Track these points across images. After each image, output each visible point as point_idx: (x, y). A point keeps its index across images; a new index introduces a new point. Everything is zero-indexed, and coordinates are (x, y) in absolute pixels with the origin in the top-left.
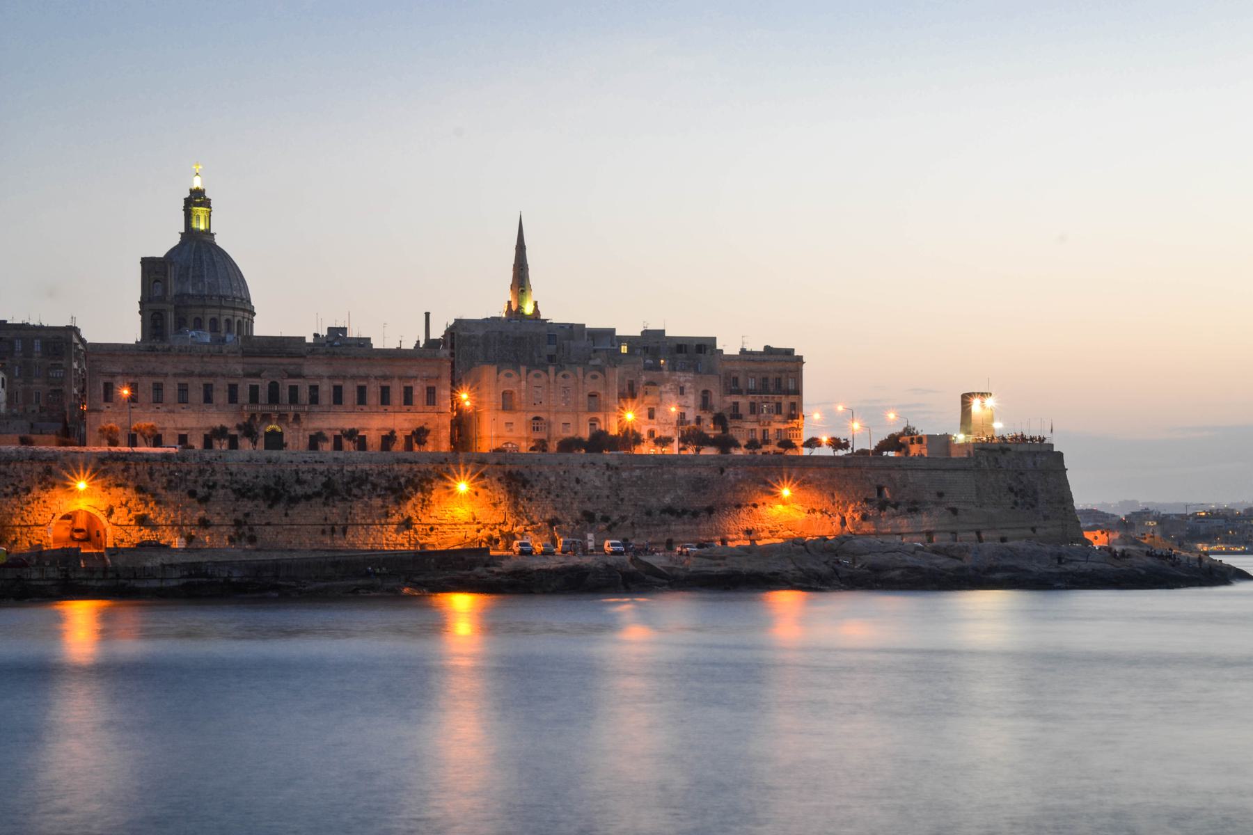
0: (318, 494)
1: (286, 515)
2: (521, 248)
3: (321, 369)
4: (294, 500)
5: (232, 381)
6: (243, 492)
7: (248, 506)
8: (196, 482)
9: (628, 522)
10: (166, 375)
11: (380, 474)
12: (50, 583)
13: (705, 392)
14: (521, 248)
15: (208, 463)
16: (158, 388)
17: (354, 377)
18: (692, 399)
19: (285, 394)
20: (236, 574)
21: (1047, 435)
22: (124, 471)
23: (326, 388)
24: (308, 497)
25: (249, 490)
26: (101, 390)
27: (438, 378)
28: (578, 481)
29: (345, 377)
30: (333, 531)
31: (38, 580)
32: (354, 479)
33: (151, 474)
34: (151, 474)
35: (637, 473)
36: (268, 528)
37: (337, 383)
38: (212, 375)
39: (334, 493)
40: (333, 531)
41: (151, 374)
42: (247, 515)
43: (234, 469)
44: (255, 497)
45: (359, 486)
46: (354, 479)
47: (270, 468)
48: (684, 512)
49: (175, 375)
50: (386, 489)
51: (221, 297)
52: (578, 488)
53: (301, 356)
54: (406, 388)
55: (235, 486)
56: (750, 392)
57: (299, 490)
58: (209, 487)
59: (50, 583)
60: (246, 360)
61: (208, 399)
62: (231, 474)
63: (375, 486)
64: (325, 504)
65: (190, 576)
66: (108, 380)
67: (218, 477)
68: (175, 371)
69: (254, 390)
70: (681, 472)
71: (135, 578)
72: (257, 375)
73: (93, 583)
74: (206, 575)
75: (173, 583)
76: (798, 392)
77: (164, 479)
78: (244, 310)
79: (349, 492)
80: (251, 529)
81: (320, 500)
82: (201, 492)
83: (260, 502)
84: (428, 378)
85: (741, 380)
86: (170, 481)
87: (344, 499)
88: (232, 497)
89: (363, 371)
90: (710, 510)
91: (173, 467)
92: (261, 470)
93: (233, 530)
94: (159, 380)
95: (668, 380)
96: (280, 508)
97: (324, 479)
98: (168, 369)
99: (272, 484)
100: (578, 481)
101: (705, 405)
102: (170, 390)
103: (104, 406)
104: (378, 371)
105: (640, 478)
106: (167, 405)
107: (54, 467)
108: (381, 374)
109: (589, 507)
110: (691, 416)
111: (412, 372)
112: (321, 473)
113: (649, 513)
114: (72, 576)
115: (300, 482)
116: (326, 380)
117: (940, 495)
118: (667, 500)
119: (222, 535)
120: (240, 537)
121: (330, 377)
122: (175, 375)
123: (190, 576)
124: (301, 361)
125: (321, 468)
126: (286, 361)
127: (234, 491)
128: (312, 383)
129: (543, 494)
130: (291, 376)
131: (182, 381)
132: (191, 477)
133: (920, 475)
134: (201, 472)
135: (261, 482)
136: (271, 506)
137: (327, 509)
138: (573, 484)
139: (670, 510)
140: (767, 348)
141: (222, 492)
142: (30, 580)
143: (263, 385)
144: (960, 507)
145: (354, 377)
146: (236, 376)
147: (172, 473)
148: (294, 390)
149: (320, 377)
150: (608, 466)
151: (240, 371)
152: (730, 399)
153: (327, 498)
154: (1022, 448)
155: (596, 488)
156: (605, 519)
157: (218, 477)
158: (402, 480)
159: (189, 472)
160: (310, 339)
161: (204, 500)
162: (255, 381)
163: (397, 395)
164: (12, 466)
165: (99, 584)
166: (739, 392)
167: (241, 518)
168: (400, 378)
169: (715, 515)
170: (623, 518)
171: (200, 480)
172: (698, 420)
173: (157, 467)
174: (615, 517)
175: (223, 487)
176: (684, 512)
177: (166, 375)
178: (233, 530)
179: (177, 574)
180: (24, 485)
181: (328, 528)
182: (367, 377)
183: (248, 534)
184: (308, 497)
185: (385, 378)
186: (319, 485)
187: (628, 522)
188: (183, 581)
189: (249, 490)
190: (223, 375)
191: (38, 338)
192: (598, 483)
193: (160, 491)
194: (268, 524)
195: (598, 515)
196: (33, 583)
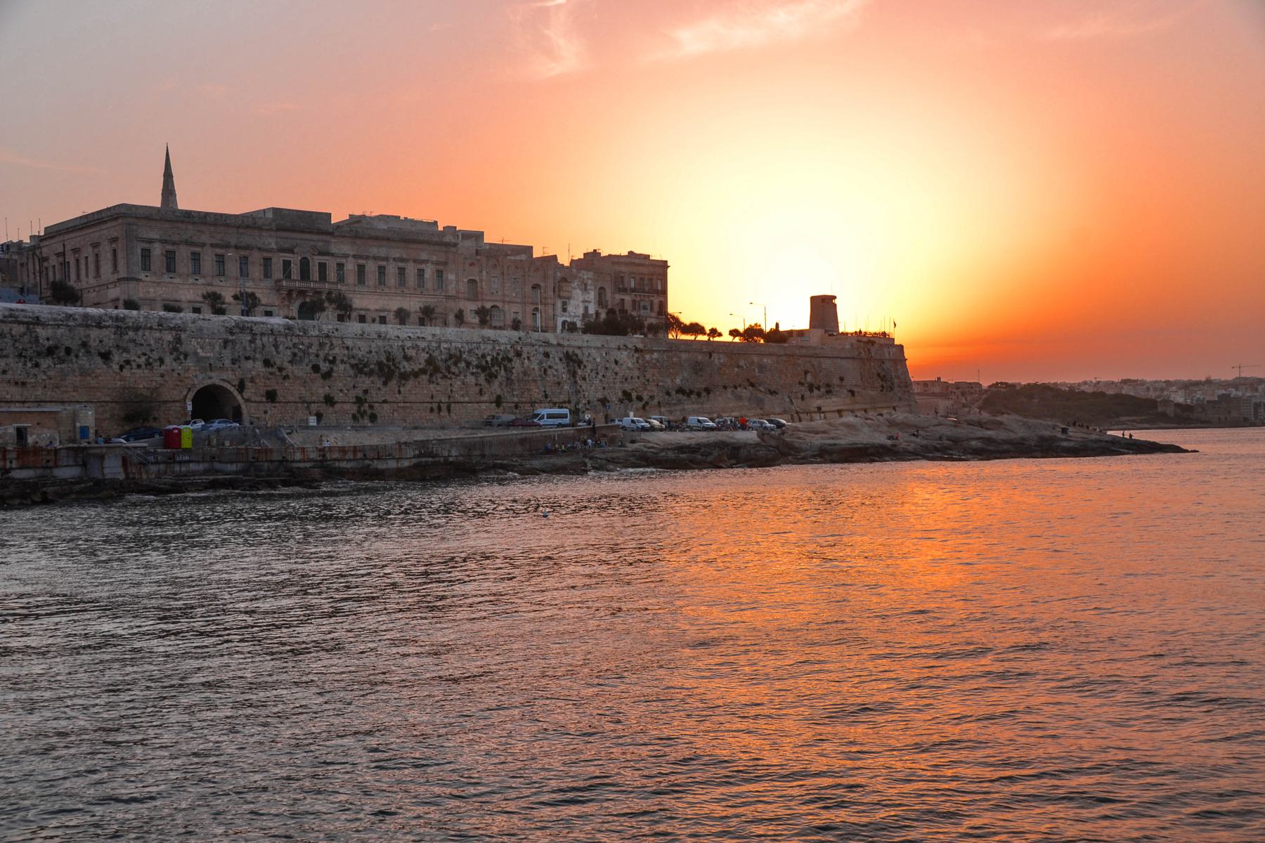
0: (423, 371)
1: (399, 392)
2: (168, 175)
3: (347, 249)
4: (405, 377)
6: (360, 368)
7: (365, 382)
8: (317, 356)
9: (655, 401)
10: (203, 245)
12: (308, 465)
13: (601, 288)
14: (168, 175)
15: (328, 336)
16: (196, 258)
17: (375, 258)
18: (592, 296)
19: (315, 273)
20: (454, 453)
21: (888, 329)
22: (251, 342)
23: (350, 266)
24: (415, 375)
25: (365, 366)
26: (138, 257)
27: (445, 264)
28: (616, 362)
29: (367, 258)
31: (299, 462)
32: (451, 357)
33: (276, 346)
34: (276, 346)
37: (361, 262)
38: (247, 248)
39: (437, 369)
40: (440, 409)
41: (189, 243)
42: (366, 392)
43: (349, 343)
44: (371, 373)
45: (455, 364)
46: (451, 357)
47: (380, 343)
48: (691, 392)
49: (212, 245)
50: (477, 367)
52: (617, 369)
54: (419, 270)
55: (353, 362)
56: (633, 290)
57: (407, 367)
59: (308, 465)
60: (279, 234)
62: (348, 348)
63: (468, 364)
64: (430, 382)
65: (420, 455)
66: (146, 246)
67: (337, 351)
68: (214, 241)
69: (287, 264)
70: (684, 356)
71: (378, 459)
72: (291, 251)
73: (343, 465)
74: (431, 455)
75: (406, 464)
76: (664, 292)
77: (289, 352)
79: (448, 369)
80: (371, 407)
81: (425, 377)
82: (324, 367)
83: (375, 378)
84: (438, 263)
85: (626, 279)
86: (295, 355)
87: (444, 377)
88: (351, 372)
90: (708, 391)
91: (295, 340)
92: (373, 345)
93: (355, 407)
94: (197, 249)
95: (576, 277)
96: (393, 384)
97: (427, 356)
100: (616, 362)
101: (601, 302)
103: (142, 276)
105: (657, 360)
107: (183, 336)
108: (397, 255)
109: (627, 387)
110: (592, 311)
111: (424, 256)
112: (423, 350)
113: (668, 394)
114: (328, 456)
115: (407, 358)
116: (350, 259)
120: (363, 414)
121: (354, 256)
122: (212, 245)
123: (420, 455)
125: (423, 344)
126: (315, 237)
127: (352, 366)
128: (339, 260)
130: (320, 254)
131: (219, 251)
132: (313, 350)
133: (828, 361)
134: (321, 345)
135: (374, 358)
136: (385, 384)
138: (613, 365)
139: (680, 391)
141: (342, 367)
142: (293, 461)
143: (295, 260)
145: (375, 258)
146: (270, 251)
147: (295, 345)
148: (322, 266)
149: (346, 256)
150: (637, 350)
152: (618, 297)
153: (431, 375)
154: (882, 341)
155: (629, 369)
157: (337, 351)
158: (489, 358)
159: (310, 345)
161: (327, 375)
162: (288, 256)
164: (140, 333)
166: (624, 290)
167: (361, 394)
168: (415, 261)
169: (711, 395)
170: (652, 397)
171: (322, 354)
173: (281, 339)
174: (646, 398)
175: (342, 362)
176: (691, 392)
178: (355, 407)
179: (410, 453)
181: (435, 406)
182: (386, 259)
183: (369, 412)
184: (415, 375)
185: (402, 260)
186: (422, 361)
187: (655, 401)
188: (415, 461)
189: (365, 366)
190: (259, 249)
192: (630, 365)
193: (286, 364)
194: (385, 402)
195: (634, 395)
196: (295, 465)
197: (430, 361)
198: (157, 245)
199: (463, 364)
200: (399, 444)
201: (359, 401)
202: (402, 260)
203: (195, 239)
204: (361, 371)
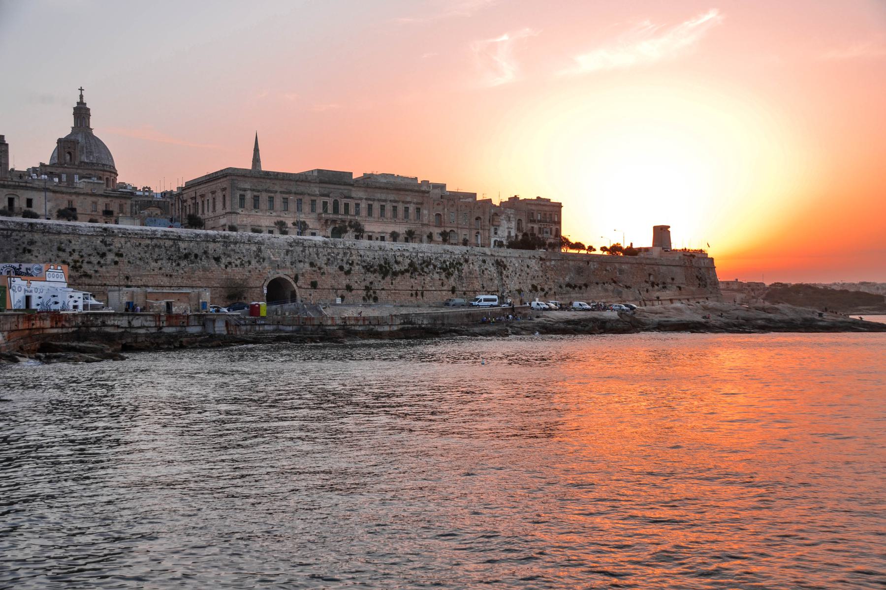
0: (407, 271)
2: (256, 150)
3: (361, 194)
4: (395, 274)
5: (313, 198)
6: (368, 268)
7: (371, 277)
10: (276, 192)
11: (436, 258)
14: (256, 150)
15: (349, 248)
16: (271, 199)
17: (379, 200)
18: (513, 224)
22: (302, 251)
23: (363, 205)
24: (402, 273)
25: (371, 267)
28: (528, 266)
29: (374, 200)
30: (417, 294)
32: (424, 262)
33: (317, 254)
34: (317, 254)
35: (553, 263)
36: (383, 292)
37: (370, 202)
38: (302, 194)
39: (415, 270)
40: (417, 294)
42: (371, 283)
43: (362, 253)
44: (375, 272)
45: (427, 266)
46: (424, 262)
47: (381, 253)
49: (281, 192)
51: (104, 165)
52: (528, 271)
53: (352, 185)
56: (539, 221)
57: (397, 268)
58: (351, 264)
60: (321, 185)
61: (382, 214)
63: (435, 266)
64: (411, 277)
65: (404, 323)
67: (354, 257)
70: (571, 263)
73: (357, 328)
75: (395, 328)
76: (559, 223)
77: (325, 258)
78: (111, 172)
79: (422, 269)
80: (375, 293)
81: (408, 275)
82: (346, 267)
83: (377, 275)
86: (329, 259)
87: (420, 274)
88: (363, 271)
89: (383, 197)
90: (586, 285)
91: (329, 251)
92: (376, 254)
98: (277, 188)
99: (382, 263)
100: (528, 266)
102: (278, 202)
103: (239, 211)
104: (391, 197)
106: (276, 211)
109: (535, 282)
110: (513, 234)
111: (409, 199)
113: (561, 287)
115: (397, 262)
116: (364, 201)
117: (673, 279)
118: (567, 279)
119: (359, 295)
120: (369, 297)
121: (366, 199)
122: (281, 192)
123: (404, 323)
124: (350, 188)
125: (407, 254)
126: (342, 187)
127: (363, 267)
128: (357, 202)
129: (513, 274)
130: (346, 197)
132: (340, 257)
133: (664, 268)
134: (345, 254)
135: (377, 262)
136: (383, 278)
137: (412, 280)
138: (526, 269)
140: (538, 198)
141: (357, 267)
142: (327, 325)
143: (330, 201)
144: (682, 286)
145: (379, 200)
147: (329, 254)
148: (347, 205)
149: (361, 199)
150: (541, 259)
151: (317, 193)
152: (530, 225)
154: (700, 255)
156: (542, 290)
157: (354, 257)
158: (448, 263)
159: (338, 254)
160: (175, 190)
161: (348, 273)
162: (326, 199)
163: (389, 213)
164: (238, 245)
165: (360, 329)
166: (533, 221)
168: (403, 202)
172: (516, 236)
173: (320, 250)
174: (546, 289)
175: (357, 264)
176: (576, 286)
177: (276, 192)
179: (398, 322)
180: (246, 259)
181: (414, 292)
182: (385, 201)
184: (402, 273)
185: (395, 201)
186: (406, 264)
187: (552, 292)
188: (400, 327)
189: (371, 267)
191: (76, 174)
194: (383, 289)
195: (539, 287)
197: (411, 264)
198: (278, 195)
199: (431, 267)
200: (391, 316)
201: (367, 289)
202: (395, 201)
203: (271, 189)
204: (368, 270)
